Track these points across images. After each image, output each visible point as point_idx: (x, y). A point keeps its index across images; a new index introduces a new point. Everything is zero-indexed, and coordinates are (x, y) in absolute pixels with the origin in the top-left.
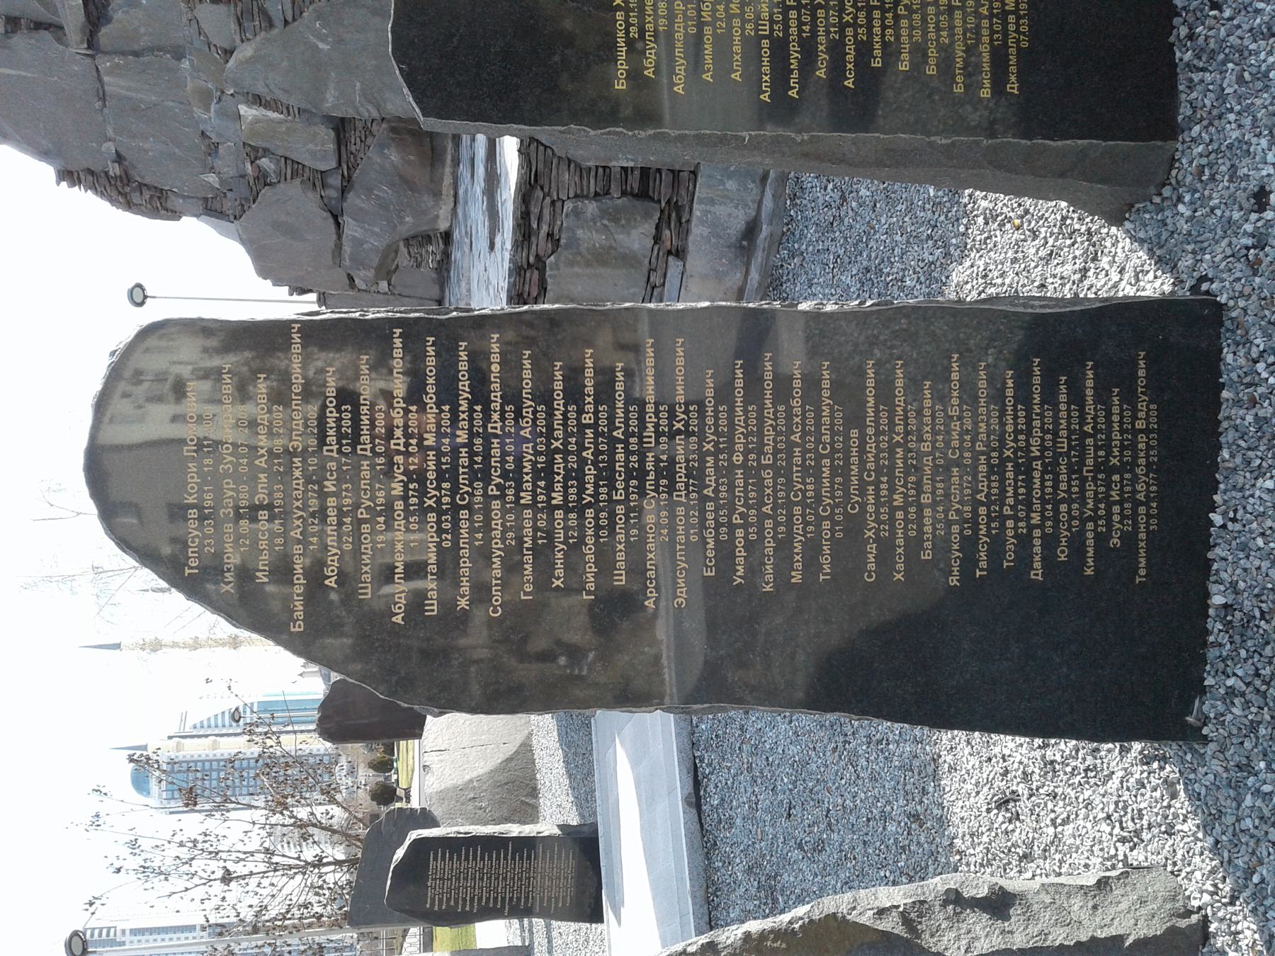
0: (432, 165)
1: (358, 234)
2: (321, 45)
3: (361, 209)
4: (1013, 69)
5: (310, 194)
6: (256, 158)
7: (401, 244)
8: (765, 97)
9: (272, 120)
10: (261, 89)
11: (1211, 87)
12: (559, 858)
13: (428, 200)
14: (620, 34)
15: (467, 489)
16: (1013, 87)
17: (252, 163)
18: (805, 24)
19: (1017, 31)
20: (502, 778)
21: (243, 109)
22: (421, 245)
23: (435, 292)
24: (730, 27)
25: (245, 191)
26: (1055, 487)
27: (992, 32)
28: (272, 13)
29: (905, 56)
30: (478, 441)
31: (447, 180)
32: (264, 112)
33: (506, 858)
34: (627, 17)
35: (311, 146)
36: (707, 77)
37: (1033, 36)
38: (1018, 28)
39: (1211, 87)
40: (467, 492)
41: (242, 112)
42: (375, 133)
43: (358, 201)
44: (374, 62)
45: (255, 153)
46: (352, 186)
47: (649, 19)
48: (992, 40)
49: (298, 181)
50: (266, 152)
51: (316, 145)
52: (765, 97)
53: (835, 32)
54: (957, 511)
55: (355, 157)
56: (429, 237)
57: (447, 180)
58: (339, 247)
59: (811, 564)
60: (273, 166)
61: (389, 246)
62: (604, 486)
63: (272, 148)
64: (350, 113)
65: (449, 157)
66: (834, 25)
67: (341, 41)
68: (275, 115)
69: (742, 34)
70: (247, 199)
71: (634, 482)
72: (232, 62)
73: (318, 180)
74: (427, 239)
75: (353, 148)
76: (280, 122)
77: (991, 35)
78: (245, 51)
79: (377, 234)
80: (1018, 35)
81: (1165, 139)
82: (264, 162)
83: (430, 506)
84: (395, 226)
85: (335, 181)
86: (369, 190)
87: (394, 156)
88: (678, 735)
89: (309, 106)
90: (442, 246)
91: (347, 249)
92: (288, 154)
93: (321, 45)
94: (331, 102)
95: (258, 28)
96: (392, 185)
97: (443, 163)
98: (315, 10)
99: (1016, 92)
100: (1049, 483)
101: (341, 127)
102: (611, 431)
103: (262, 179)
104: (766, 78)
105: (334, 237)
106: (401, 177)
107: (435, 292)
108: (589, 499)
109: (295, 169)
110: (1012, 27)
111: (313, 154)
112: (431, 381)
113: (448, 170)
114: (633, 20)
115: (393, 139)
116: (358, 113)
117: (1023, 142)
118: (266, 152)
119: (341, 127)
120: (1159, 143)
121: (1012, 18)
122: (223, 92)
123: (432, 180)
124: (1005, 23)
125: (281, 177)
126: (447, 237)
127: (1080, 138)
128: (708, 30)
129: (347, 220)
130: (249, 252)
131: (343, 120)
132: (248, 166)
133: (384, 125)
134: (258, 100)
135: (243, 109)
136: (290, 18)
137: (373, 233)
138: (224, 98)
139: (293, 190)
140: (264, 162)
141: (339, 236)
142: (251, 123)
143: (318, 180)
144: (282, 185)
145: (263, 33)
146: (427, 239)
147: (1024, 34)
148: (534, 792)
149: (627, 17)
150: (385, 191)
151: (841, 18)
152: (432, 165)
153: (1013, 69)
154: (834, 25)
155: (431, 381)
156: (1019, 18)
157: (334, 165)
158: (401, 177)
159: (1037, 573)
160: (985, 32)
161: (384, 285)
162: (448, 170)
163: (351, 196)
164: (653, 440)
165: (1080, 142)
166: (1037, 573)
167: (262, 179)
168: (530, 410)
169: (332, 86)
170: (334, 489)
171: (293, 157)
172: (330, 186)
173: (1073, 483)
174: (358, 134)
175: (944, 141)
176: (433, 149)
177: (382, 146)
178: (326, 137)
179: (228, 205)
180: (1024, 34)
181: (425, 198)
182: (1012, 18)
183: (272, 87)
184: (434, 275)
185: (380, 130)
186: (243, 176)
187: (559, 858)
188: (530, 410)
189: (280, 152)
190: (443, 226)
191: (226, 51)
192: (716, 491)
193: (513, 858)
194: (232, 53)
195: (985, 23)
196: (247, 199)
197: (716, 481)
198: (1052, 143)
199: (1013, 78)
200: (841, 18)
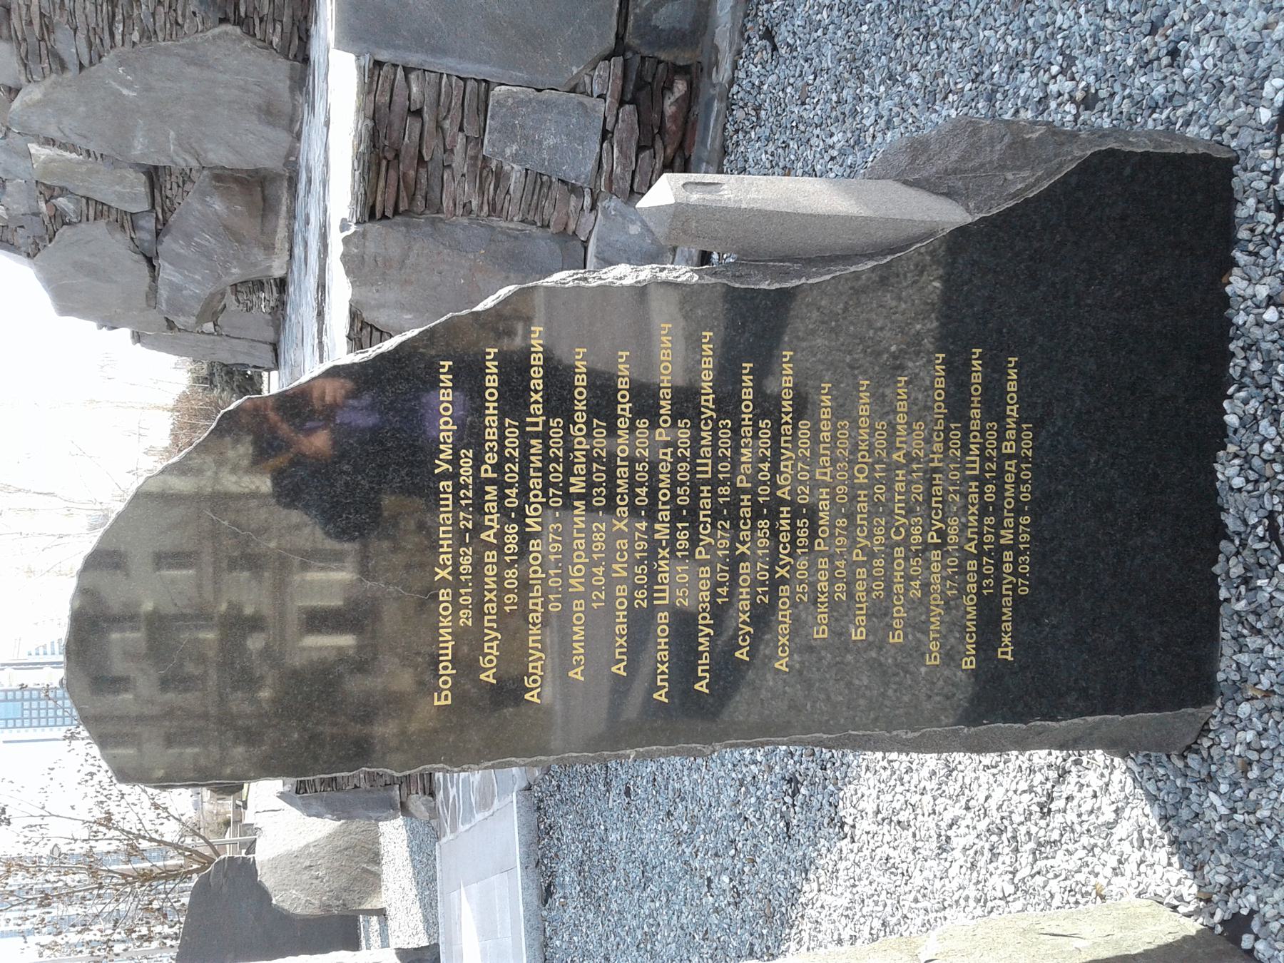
0: (263, 216)
1: (177, 278)
2: (125, 92)
3: (179, 255)
4: (1007, 626)
5: (119, 236)
6: (52, 197)
7: (229, 289)
8: (660, 696)
9: (70, 160)
10: (53, 132)
11: (1272, 663)
13: (259, 255)
14: (445, 622)
16: (1006, 651)
17: (47, 202)
18: (721, 585)
19: (1015, 573)
20: (341, 843)
21: (34, 148)
22: (252, 292)
23: (269, 335)
24: (611, 598)
25: (40, 230)
27: (982, 576)
28: (66, 57)
29: (861, 619)
31: (282, 233)
32: (60, 152)
34: (456, 595)
35: (117, 188)
36: (576, 674)
37: (1037, 582)
38: (1015, 569)
39: (1272, 663)
41: (32, 151)
42: (195, 179)
43: (174, 246)
44: (190, 111)
45: (51, 193)
46: (168, 232)
47: (489, 596)
48: (980, 587)
49: (102, 222)
50: (64, 191)
51: (124, 187)
52: (660, 696)
53: (764, 593)
54: (939, 531)
55: (171, 201)
56: (261, 283)
57: (282, 233)
58: (153, 291)
60: (72, 207)
61: (213, 295)
63: (70, 187)
64: (162, 161)
65: (284, 208)
66: (763, 584)
67: (148, 88)
68: (74, 155)
69: (630, 608)
70: (41, 238)
72: (16, 104)
73: (126, 222)
74: (259, 285)
75: (169, 193)
76: (79, 163)
77: (979, 583)
78: (32, 93)
79: (199, 282)
80: (1015, 575)
81: (1197, 705)
82: (62, 202)
84: (220, 277)
85: (149, 223)
86: (188, 237)
87: (218, 205)
88: (529, 947)
89: (113, 153)
90: (276, 295)
91: (163, 293)
92: (90, 195)
93: (125, 92)
94: (140, 148)
95: (47, 71)
96: (215, 234)
97: (277, 215)
98: (117, 56)
99: (1009, 658)
101: (154, 175)
103: (60, 219)
104: (663, 668)
105: (148, 279)
106: (226, 227)
107: (269, 335)
108: (446, 466)
109: (101, 210)
110: (1007, 568)
111: (121, 197)
113: (282, 222)
114: (466, 600)
115: (216, 188)
116: (172, 161)
117: (1016, 726)
118: (64, 191)
119: (154, 175)
120: (1190, 710)
121: (1008, 556)
122: (8, 129)
123: (263, 232)
124: (998, 564)
125: (83, 218)
126: (282, 284)
127: (1091, 714)
128: (578, 606)
129: (161, 263)
131: (156, 168)
132: (43, 205)
133: (205, 172)
134: (50, 142)
135: (34, 148)
136: (86, 62)
137: (194, 281)
138: (10, 134)
139: (99, 229)
140: (62, 202)
141: (154, 279)
142: (44, 162)
143: (126, 222)
144: (83, 225)
145: (54, 76)
146: (259, 285)
147: (1023, 576)
148: (376, 858)
149: (456, 595)
150: (207, 240)
151: (772, 572)
152: (263, 216)
153: (1007, 626)
154: (763, 584)
156: (1018, 553)
157: (146, 207)
158: (226, 227)
160: (972, 578)
161: (209, 327)
162: (282, 222)
163: (167, 240)
165: (1089, 719)
167: (60, 219)
169: (140, 134)
171: (98, 197)
172: (142, 228)
174: (174, 179)
175: (910, 735)
176: (264, 199)
177: (203, 194)
178: (139, 185)
179: (20, 238)
180: (1023, 576)
181: (255, 250)
182: (1008, 556)
183: (67, 131)
184: (269, 317)
185: (202, 178)
186: (37, 214)
189: (81, 192)
190: (278, 273)
191: (10, 89)
194: (18, 91)
195: (972, 565)
196: (41, 238)
198: (1054, 724)
199: (1006, 639)
200: (772, 572)
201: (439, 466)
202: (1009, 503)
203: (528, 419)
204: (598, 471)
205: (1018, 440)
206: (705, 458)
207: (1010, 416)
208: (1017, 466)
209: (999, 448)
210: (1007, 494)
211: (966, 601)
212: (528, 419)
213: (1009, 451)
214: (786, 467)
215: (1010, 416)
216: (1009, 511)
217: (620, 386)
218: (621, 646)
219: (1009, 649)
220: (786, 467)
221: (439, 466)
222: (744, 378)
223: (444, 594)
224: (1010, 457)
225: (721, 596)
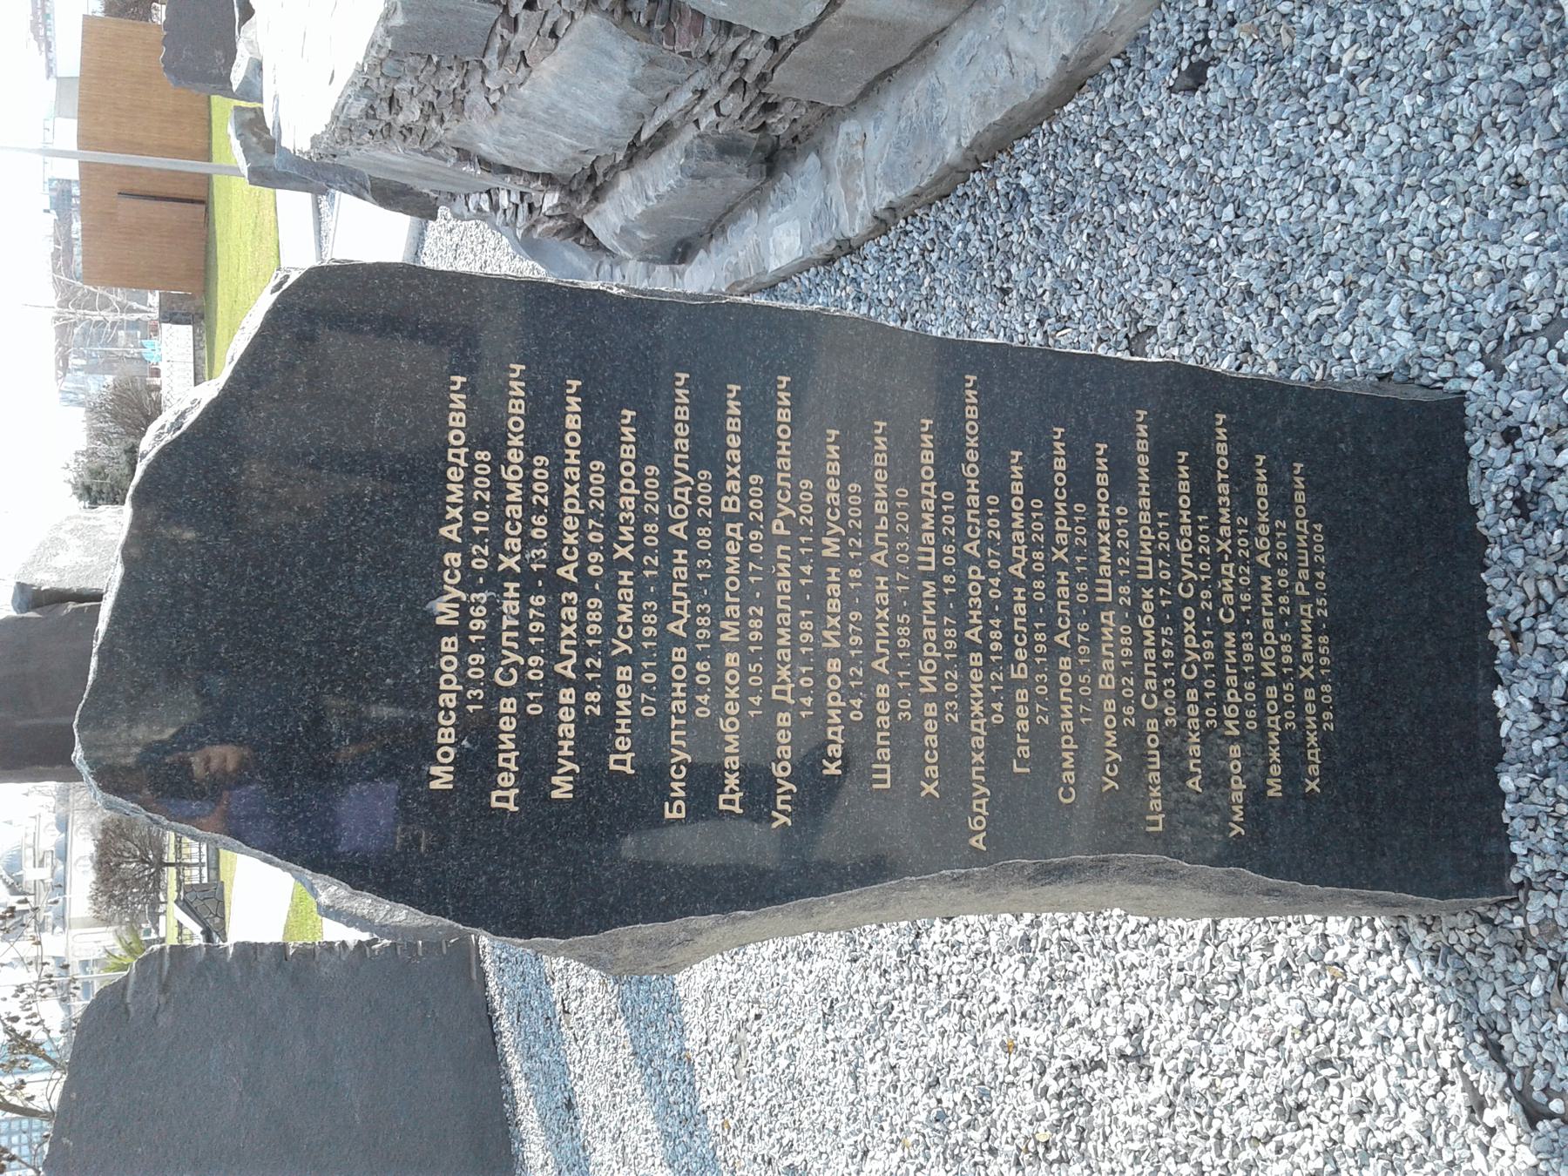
12: (1244, 501)
15: (514, 657)
26: (610, 622)
30: (540, 520)
33: (948, 477)
40: (515, 664)
58: (598, 246)
59: (1292, 777)
62: (807, 618)
71: (537, 601)
83: (623, 557)
100: (756, 624)
102: (1005, 566)
112: (972, 443)
130: (363, 265)
155: (972, 443)
159: (505, 795)
164: (1109, 591)
166: (505, 795)
168: (687, 490)
170: (837, 644)
173: (1321, 651)
187: (1244, 501)
188: (687, 490)
192: (690, 627)
193: (995, 482)
197: (691, 608)
201: (616, 647)
202: (733, 584)
203: (875, 766)
204: (595, 529)
205: (745, 496)
206: (883, 762)
207: (1304, 617)
208: (744, 533)
209: (715, 506)
210: (729, 570)
211: (724, 726)
212: (875, 766)
213: (730, 509)
214: (980, 806)
215: (1304, 617)
216: (733, 595)
217: (623, 455)
218: (569, 637)
219: (737, 797)
220: (980, 806)
221: (616, 647)
222: (454, 396)
223: (449, 644)
224: (733, 518)
225: (805, 576)
